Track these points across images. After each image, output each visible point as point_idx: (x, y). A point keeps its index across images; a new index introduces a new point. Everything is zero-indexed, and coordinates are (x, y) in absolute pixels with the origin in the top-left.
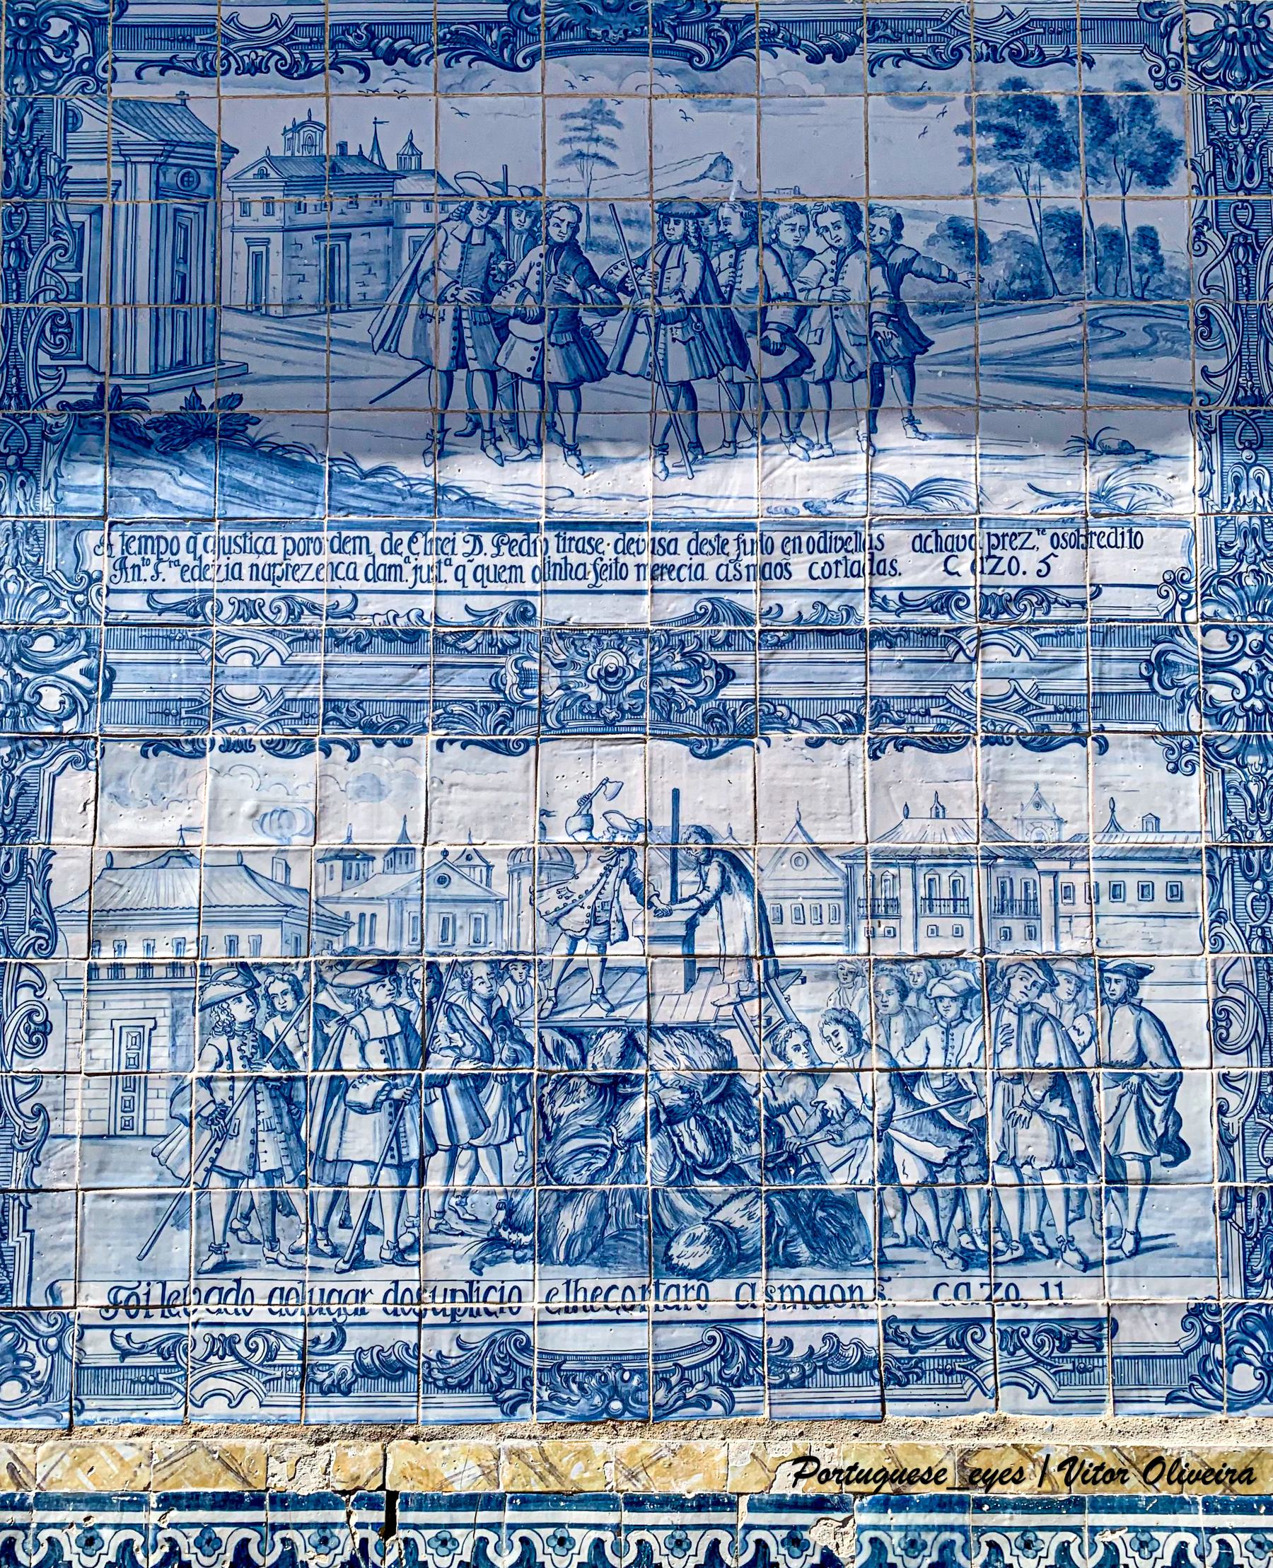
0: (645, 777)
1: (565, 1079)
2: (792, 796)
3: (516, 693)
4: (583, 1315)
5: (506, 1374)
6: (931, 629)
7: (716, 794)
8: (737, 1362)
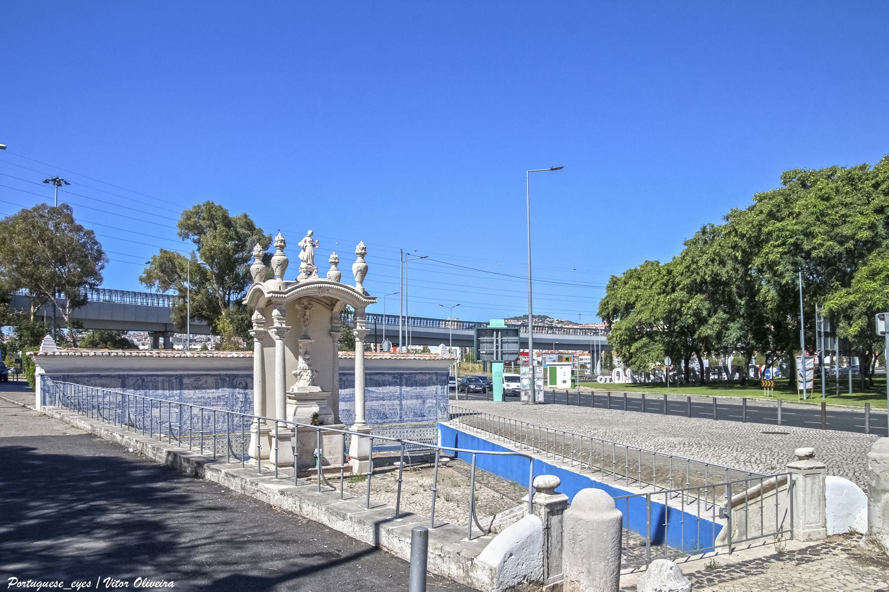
0: (381, 402)
1: (379, 413)
2: (387, 402)
3: (377, 399)
4: (380, 421)
5: (377, 423)
6: (390, 396)
7: (384, 403)
8: (384, 423)
